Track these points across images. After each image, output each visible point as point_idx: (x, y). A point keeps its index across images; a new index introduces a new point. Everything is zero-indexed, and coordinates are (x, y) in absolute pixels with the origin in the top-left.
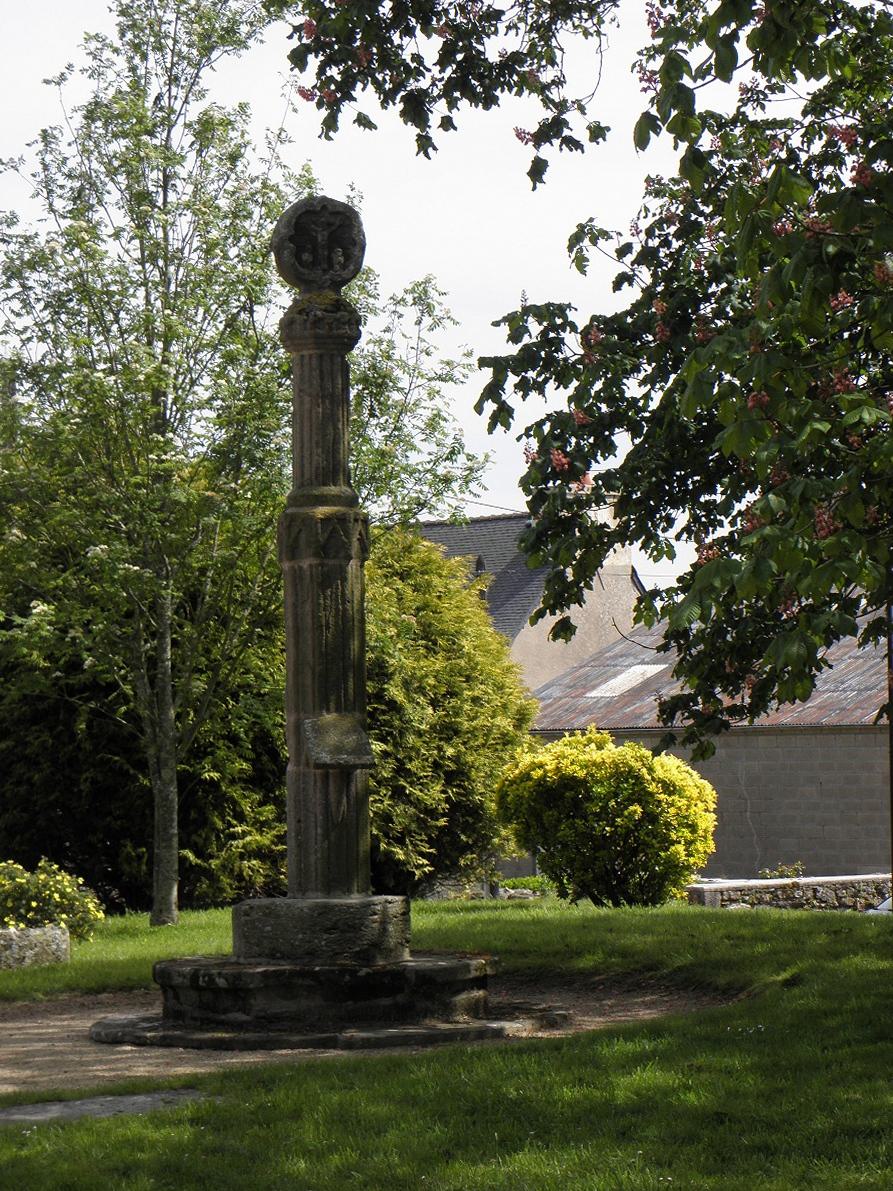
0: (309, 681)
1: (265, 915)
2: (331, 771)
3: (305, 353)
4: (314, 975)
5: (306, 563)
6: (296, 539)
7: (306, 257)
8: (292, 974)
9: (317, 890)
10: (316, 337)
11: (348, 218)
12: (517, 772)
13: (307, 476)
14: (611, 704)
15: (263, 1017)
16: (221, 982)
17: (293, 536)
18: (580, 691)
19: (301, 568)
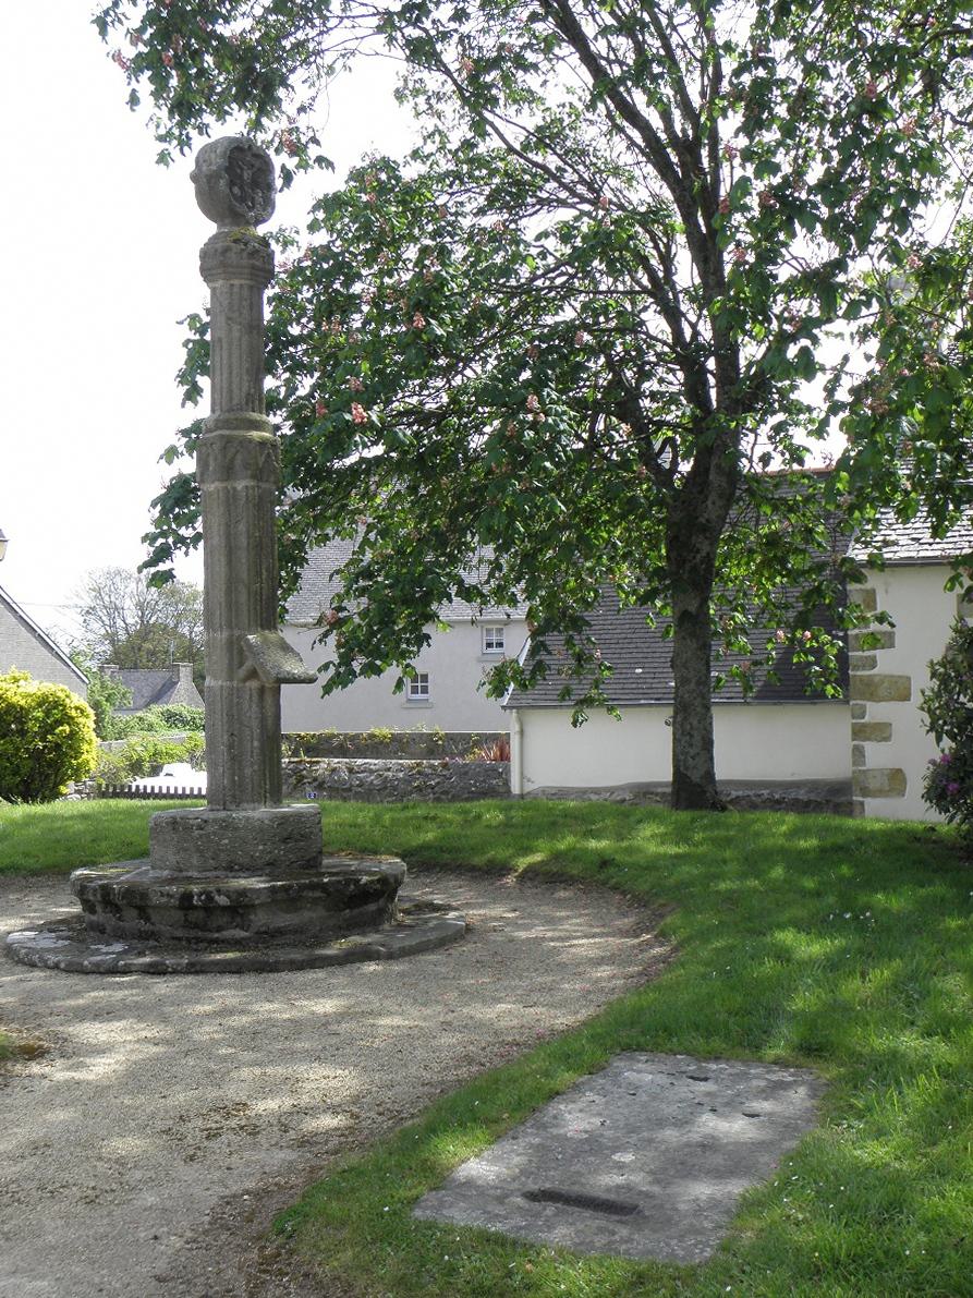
0: (243, 598)
1: (221, 828)
3: (236, 282)
4: (323, 887)
5: (240, 485)
6: (232, 461)
10: (253, 267)
13: (235, 402)
15: (265, 933)
17: (229, 457)
19: (235, 489)
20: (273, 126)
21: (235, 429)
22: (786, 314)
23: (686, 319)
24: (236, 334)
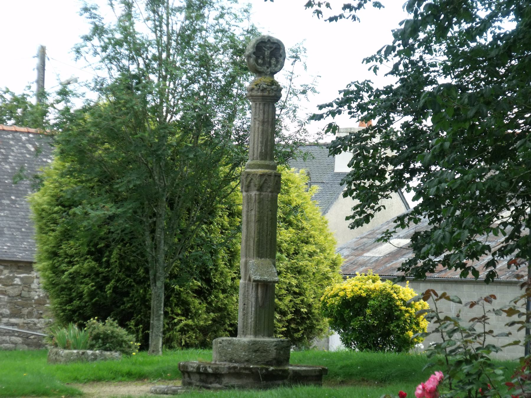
0: (252, 244)
1: (229, 343)
2: (260, 283)
7: (260, 61)
8: (241, 368)
9: (251, 334)
11: (280, 46)
12: (332, 292)
13: (255, 156)
14: (378, 262)
16: (210, 370)
18: (360, 252)
20: (27, 92)
21: (252, 168)
22: (427, 51)
23: (499, 53)
24: (257, 125)
